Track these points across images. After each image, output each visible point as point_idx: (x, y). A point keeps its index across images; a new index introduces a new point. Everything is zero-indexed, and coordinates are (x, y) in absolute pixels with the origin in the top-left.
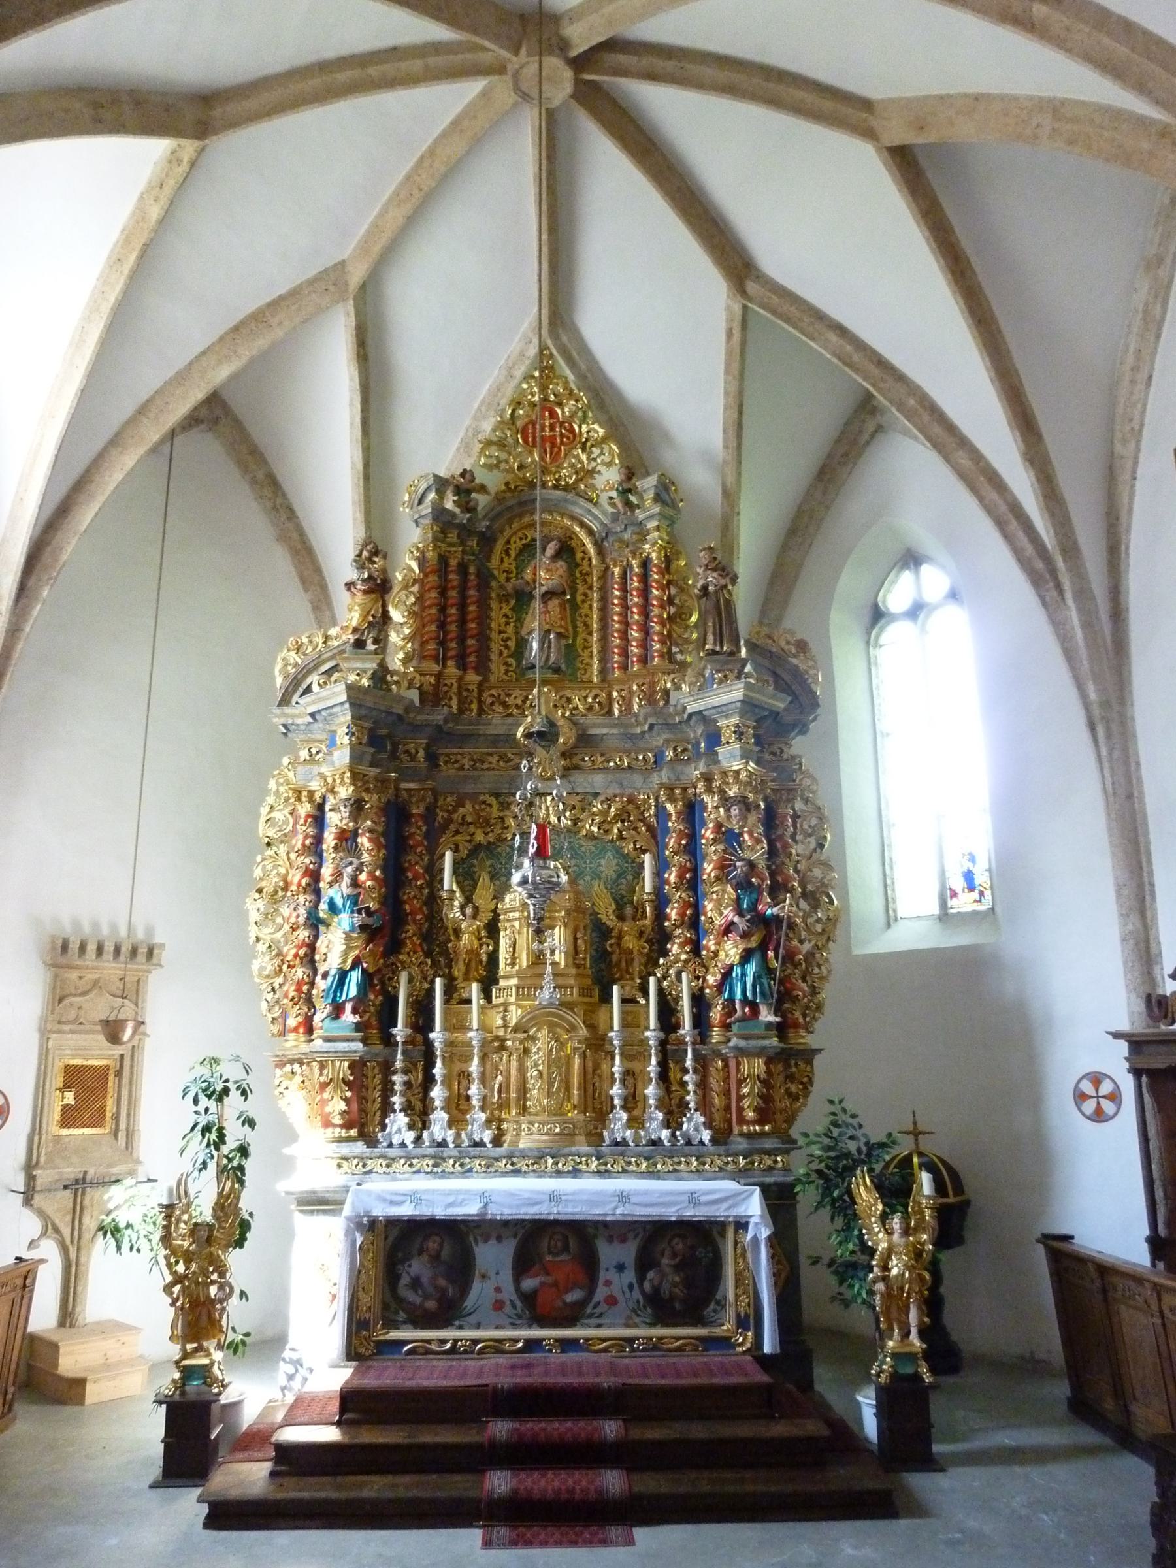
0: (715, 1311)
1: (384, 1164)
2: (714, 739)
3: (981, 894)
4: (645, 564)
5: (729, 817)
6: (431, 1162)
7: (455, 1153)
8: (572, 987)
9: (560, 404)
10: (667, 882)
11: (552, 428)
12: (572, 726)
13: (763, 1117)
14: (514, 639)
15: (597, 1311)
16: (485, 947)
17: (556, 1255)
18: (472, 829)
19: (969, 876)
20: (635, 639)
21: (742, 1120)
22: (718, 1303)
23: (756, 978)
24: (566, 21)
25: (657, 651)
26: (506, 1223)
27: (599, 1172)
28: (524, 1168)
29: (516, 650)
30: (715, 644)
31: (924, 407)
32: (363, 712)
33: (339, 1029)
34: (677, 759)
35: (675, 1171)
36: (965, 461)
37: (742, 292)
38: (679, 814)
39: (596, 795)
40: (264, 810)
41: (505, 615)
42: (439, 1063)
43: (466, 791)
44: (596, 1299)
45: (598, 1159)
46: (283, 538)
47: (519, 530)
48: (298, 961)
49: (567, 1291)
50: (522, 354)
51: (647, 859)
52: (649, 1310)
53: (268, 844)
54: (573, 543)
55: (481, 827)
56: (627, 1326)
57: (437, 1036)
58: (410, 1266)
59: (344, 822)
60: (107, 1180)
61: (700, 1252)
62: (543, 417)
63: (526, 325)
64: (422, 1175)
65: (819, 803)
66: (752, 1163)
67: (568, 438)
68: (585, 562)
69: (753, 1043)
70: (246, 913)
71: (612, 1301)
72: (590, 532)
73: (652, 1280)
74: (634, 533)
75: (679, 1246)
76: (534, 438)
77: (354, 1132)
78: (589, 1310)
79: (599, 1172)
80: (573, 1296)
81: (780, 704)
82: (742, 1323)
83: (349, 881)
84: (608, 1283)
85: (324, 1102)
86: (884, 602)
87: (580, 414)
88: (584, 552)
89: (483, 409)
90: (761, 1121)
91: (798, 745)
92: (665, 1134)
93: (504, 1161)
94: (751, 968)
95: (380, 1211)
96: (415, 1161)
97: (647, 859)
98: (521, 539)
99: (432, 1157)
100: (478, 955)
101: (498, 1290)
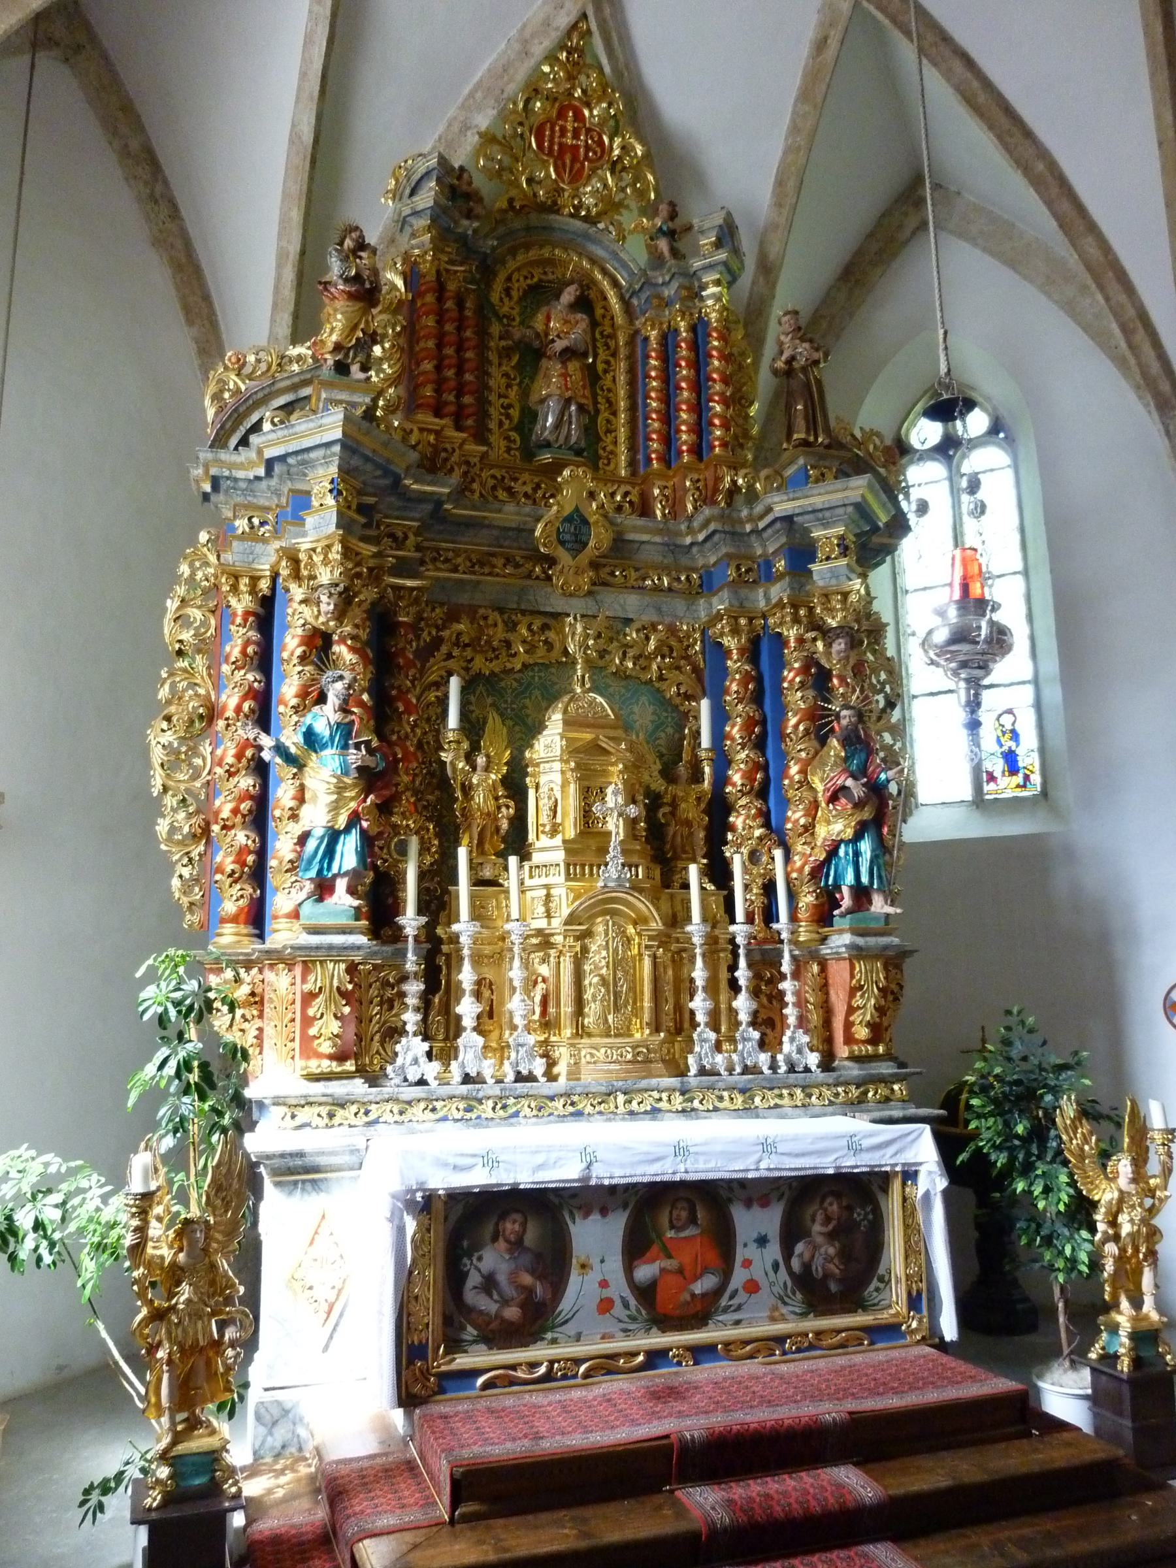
0: (877, 1290)
1: (396, 1110)
3: (1027, 778)
4: (699, 328)
5: (828, 654)
6: (462, 1106)
7: (496, 1090)
8: (637, 867)
9: (588, 105)
12: (607, 525)
14: (517, 406)
15: (735, 1302)
16: (504, 809)
17: (679, 1229)
18: (468, 653)
19: (1010, 759)
20: (684, 422)
21: (849, 1039)
22: (881, 1279)
25: (718, 439)
26: (613, 1189)
27: (684, 1111)
28: (589, 1109)
29: (521, 422)
30: (808, 432)
31: (1052, 174)
32: (356, 461)
33: (323, 914)
35: (777, 1106)
36: (1093, 251)
38: (742, 651)
39: (628, 621)
40: (172, 605)
41: (506, 375)
43: (461, 601)
45: (683, 1093)
46: (159, 242)
47: (524, 265)
48: (238, 819)
49: (696, 1278)
50: (547, 23)
51: (705, 705)
52: (799, 1296)
53: (180, 653)
54: (592, 294)
55: (482, 652)
56: (773, 1319)
57: (464, 927)
58: (480, 1259)
59: (322, 619)
60: (1114, 1209)
62: (565, 118)
64: (449, 1124)
66: (866, 1093)
67: (595, 153)
68: (607, 322)
69: (872, 941)
70: (146, 750)
71: (752, 1287)
72: (615, 284)
73: (801, 1255)
74: (681, 287)
76: (551, 143)
78: (724, 1302)
79: (684, 1111)
80: (705, 1284)
82: (914, 1302)
83: (337, 702)
84: (747, 1263)
85: (307, 1021)
86: (907, 435)
87: (612, 123)
88: (605, 308)
89: (479, 95)
92: (763, 1059)
93: (562, 1101)
94: (866, 846)
95: (442, 1181)
96: (438, 1105)
98: (526, 278)
99: (463, 1098)
100: (496, 819)
101: (604, 1284)
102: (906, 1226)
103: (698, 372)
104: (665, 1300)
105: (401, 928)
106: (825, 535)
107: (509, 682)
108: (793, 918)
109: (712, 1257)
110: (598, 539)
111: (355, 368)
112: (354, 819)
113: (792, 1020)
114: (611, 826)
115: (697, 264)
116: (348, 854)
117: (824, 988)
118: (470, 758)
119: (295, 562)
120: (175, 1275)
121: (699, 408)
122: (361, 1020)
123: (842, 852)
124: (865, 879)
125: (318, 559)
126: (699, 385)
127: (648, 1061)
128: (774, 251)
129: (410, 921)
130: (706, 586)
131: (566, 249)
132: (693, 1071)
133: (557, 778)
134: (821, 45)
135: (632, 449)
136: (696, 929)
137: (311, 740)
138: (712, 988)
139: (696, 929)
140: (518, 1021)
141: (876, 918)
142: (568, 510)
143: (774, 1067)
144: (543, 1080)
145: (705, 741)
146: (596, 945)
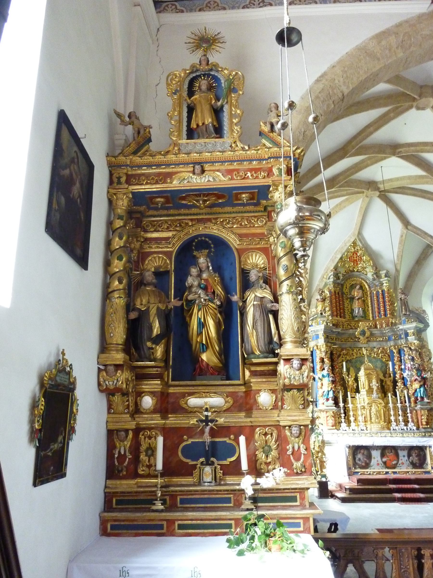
2: (407, 335)
7: (358, 432)
10: (396, 369)
11: (356, 257)
13: (427, 424)
18: (346, 356)
21: (422, 425)
23: (424, 392)
24: (379, 183)
26: (378, 446)
34: (395, 339)
37: (407, 228)
38: (397, 352)
39: (375, 347)
42: (392, 411)
44: (399, 463)
50: (349, 240)
51: (390, 363)
57: (350, 406)
61: (421, 453)
63: (350, 233)
65: (429, 348)
69: (424, 406)
71: (403, 464)
72: (367, 282)
75: (417, 452)
77: (334, 427)
78: (398, 465)
80: (394, 462)
81: (421, 326)
84: (401, 460)
90: (427, 425)
91: (423, 333)
92: (405, 428)
94: (422, 389)
97: (390, 363)
101: (378, 461)
102: (430, 455)
103: (384, 300)
104: (388, 464)
105: (339, 406)
106: (410, 332)
107: (354, 361)
108: (410, 402)
109: (396, 458)
110: (368, 334)
111: (323, 313)
112: (331, 388)
113: (410, 421)
114: (374, 387)
115: (381, 280)
116: (331, 395)
117: (417, 415)
118: (348, 376)
119: (317, 346)
120: (318, 452)
121: (384, 306)
122: (335, 420)
123: (417, 391)
124: (422, 395)
125: (322, 347)
126: (384, 302)
127: (384, 428)
128: (398, 268)
129: (341, 404)
130: (389, 339)
131: (356, 278)
132: (392, 429)
133: (364, 379)
134: (402, 236)
135: (373, 314)
136: (391, 405)
137: (323, 376)
138: (395, 415)
139: (391, 405)
140: (361, 421)
141: (425, 402)
142: (361, 329)
143: (407, 429)
144: (365, 430)
145: (391, 370)
146: (373, 408)
